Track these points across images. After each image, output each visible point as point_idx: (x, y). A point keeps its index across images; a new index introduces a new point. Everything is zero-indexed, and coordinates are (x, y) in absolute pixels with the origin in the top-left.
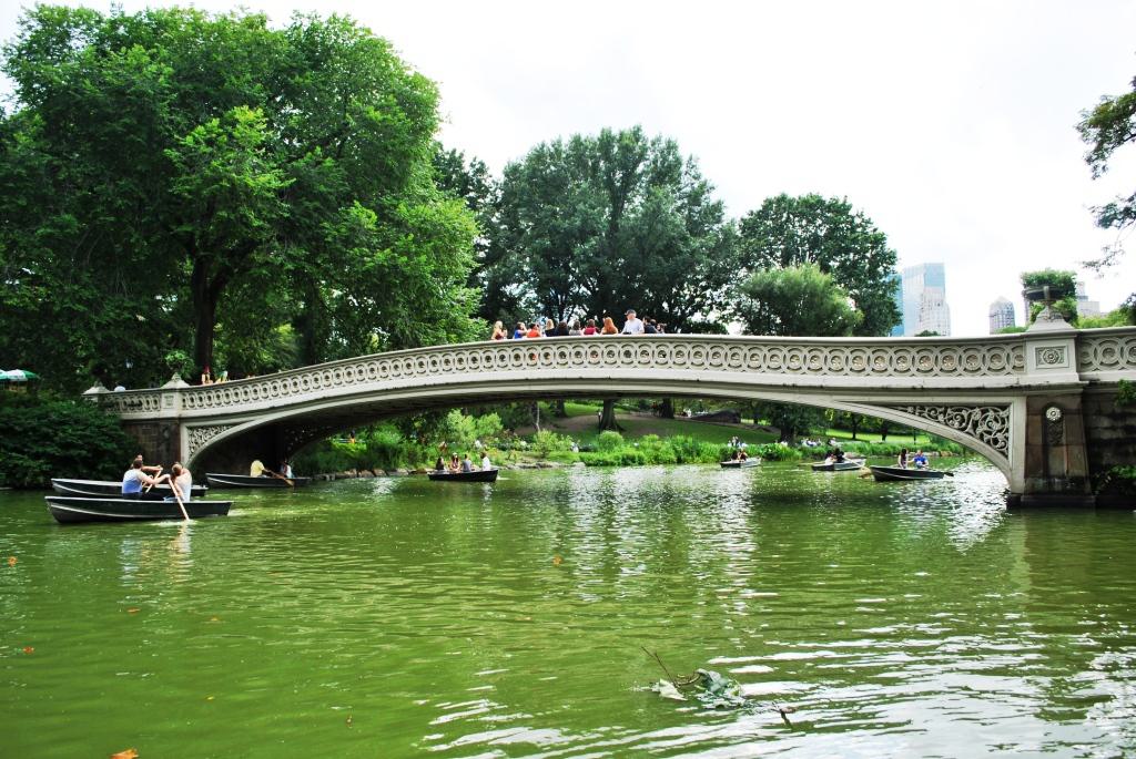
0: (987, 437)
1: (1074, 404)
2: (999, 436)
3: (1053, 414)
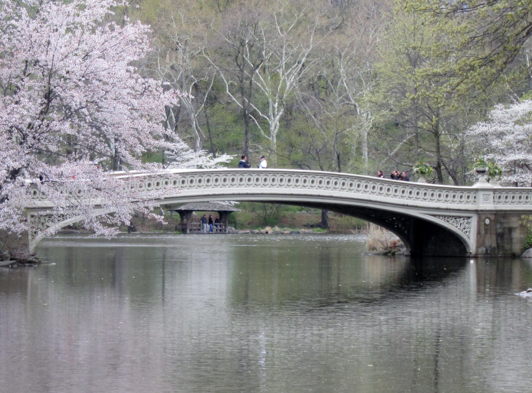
1: (493, 217)
3: (487, 221)
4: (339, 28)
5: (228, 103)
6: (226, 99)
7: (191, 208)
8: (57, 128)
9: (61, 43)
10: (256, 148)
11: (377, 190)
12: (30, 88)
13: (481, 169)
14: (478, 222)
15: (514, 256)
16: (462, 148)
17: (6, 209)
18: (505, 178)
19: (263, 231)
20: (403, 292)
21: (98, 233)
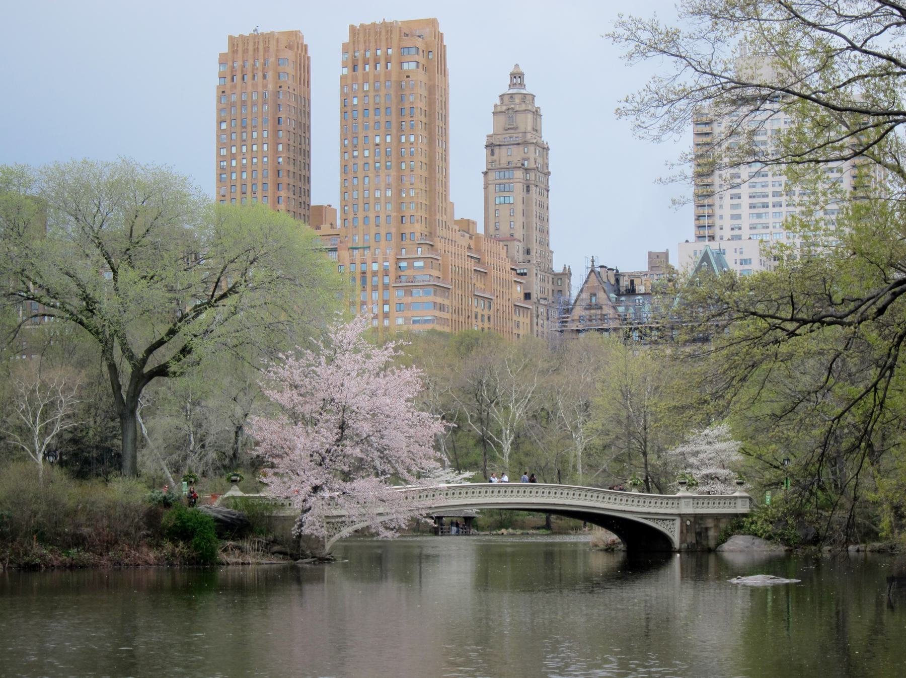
1: (692, 519)
3: (688, 523)
4: (557, 370)
5: (469, 431)
6: (468, 428)
7: (442, 515)
8: (350, 453)
9: (352, 385)
10: (492, 466)
11: (606, 500)
12: (327, 421)
13: (683, 481)
14: (681, 524)
15: (710, 551)
16: (665, 464)
17: (310, 518)
18: (700, 488)
19: (500, 532)
20: (618, 582)
21: (382, 536)
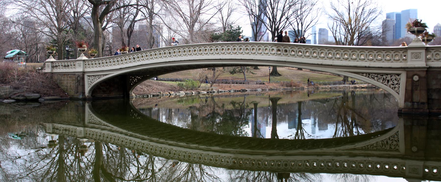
0: (392, 86)
1: (423, 74)
2: (397, 86)
3: (416, 78)
